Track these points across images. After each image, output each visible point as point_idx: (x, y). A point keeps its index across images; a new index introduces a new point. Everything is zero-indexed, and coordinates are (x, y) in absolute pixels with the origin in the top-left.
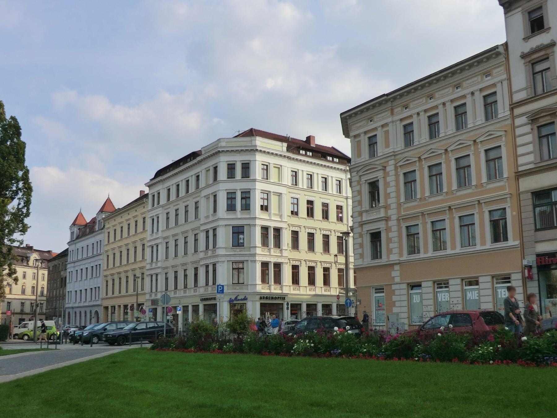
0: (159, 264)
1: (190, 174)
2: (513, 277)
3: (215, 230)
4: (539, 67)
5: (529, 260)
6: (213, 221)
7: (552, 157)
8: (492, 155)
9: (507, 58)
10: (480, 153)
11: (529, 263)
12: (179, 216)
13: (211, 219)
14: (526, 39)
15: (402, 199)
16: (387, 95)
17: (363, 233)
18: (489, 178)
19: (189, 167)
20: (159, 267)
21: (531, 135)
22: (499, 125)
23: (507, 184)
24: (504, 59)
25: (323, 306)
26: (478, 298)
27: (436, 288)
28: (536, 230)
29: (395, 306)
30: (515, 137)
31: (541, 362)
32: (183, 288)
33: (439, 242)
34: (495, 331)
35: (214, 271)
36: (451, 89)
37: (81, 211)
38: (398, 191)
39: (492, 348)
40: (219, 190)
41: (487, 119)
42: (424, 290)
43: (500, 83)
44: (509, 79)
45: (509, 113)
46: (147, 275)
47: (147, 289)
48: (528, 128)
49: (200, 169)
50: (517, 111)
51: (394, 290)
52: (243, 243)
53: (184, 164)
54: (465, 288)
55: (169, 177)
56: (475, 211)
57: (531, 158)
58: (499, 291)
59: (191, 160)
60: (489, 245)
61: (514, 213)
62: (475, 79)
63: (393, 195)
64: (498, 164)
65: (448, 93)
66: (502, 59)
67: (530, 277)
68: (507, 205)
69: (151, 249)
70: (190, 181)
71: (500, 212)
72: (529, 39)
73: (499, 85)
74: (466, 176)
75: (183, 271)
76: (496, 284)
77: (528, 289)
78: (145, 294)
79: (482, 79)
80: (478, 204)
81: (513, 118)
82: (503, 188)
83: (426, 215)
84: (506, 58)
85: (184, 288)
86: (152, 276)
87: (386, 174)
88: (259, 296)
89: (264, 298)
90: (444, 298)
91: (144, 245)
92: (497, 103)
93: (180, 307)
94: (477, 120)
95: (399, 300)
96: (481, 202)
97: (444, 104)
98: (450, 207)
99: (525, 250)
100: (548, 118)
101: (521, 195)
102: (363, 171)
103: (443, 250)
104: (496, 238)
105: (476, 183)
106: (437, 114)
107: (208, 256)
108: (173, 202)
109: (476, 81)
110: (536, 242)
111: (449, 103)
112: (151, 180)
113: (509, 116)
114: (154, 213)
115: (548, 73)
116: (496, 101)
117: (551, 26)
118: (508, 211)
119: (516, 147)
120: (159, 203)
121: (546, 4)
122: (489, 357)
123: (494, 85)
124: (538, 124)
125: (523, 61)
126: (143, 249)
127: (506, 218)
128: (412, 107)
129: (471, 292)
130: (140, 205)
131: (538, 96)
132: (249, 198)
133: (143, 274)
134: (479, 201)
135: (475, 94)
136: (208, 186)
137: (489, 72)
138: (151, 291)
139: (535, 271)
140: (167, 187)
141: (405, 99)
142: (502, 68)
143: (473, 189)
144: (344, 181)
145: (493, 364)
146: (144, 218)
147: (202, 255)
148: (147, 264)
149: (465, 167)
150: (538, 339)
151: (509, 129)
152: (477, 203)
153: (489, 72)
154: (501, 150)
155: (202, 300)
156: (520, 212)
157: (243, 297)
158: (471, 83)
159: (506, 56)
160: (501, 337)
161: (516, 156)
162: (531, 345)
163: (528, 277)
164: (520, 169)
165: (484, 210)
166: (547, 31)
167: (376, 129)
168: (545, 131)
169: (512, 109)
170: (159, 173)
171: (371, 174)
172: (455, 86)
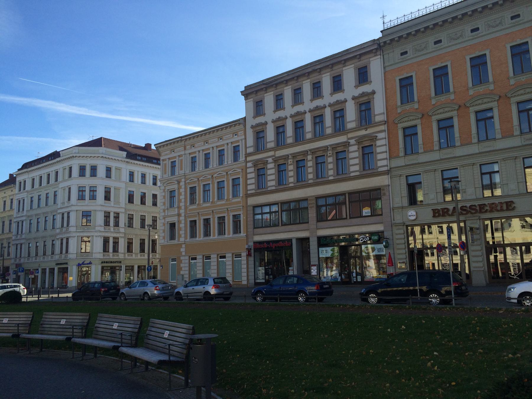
0: (23, 236)
1: (52, 170)
3: (68, 213)
6: (67, 207)
9: (245, 126)
12: (49, 199)
13: (66, 204)
15: (188, 204)
16: (181, 137)
17: (165, 223)
19: (50, 164)
20: (23, 239)
21: (254, 174)
27: (234, 257)
29: (182, 270)
32: (42, 255)
35: (67, 243)
38: (186, 198)
40: (73, 185)
42: (227, 259)
44: (245, 139)
46: (13, 245)
47: (12, 255)
49: (59, 167)
50: (249, 159)
51: (182, 260)
53: (46, 162)
55: (34, 170)
59: (52, 160)
60: (216, 237)
63: (183, 200)
69: (17, 224)
70: (59, 172)
75: (43, 242)
78: (11, 259)
85: (52, 254)
86: (17, 245)
89: (104, 262)
91: (11, 221)
93: (40, 270)
95: (184, 266)
97: (227, 144)
98: (213, 211)
107: (63, 232)
108: (36, 189)
112: (19, 170)
114: (20, 196)
117: (266, 113)
118: (242, 216)
120: (24, 189)
121: (264, 100)
126: (10, 224)
130: (8, 188)
132: (96, 191)
133: (9, 243)
134: (213, 211)
136: (64, 180)
138: (16, 257)
139: (252, 251)
140: (68, 166)
146: (12, 199)
147: (58, 231)
148: (13, 236)
155: (57, 264)
156: (247, 218)
157: (88, 262)
161: (247, 185)
164: (249, 192)
167: (175, 157)
169: (246, 157)
170: (26, 166)
171: (171, 186)
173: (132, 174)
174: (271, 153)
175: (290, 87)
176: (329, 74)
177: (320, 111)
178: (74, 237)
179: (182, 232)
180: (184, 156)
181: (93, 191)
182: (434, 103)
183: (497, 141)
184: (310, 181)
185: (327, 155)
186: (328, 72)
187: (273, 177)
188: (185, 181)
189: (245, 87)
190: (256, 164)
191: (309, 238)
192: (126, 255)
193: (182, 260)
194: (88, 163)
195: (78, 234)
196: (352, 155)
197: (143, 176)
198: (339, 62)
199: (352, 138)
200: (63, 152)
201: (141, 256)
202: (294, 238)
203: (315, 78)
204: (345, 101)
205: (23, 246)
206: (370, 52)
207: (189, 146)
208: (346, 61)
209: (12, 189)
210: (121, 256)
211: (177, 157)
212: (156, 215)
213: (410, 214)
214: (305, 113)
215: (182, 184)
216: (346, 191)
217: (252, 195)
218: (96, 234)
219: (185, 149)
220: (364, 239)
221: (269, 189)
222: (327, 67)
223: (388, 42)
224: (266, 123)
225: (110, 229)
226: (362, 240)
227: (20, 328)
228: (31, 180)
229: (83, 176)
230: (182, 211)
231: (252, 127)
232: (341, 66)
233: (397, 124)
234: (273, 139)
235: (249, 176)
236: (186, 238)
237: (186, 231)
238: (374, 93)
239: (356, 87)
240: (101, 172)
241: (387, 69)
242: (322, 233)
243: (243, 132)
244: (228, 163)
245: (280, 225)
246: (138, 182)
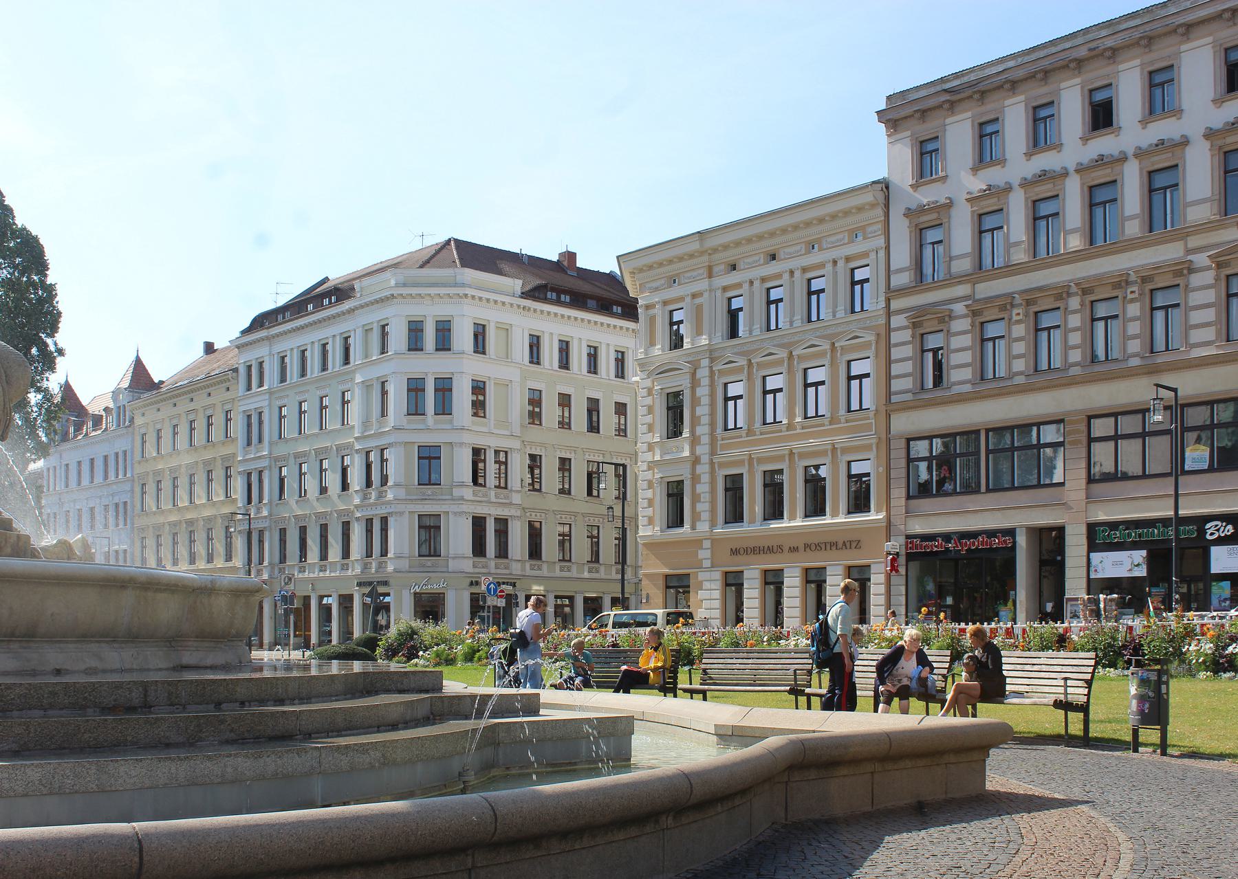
1: (331, 333)
11: (894, 548)
25: (586, 600)
33: (194, 649)
37: (68, 378)
44: (888, 248)
45: (884, 306)
52: (1138, 752)
55: (285, 333)
73: (873, 255)
81: (889, 313)
87: (695, 383)
88: (469, 581)
97: (835, 262)
102: (658, 372)
103: (998, 488)
112: (245, 332)
114: (251, 404)
139: (902, 560)
144: (630, 352)
156: (888, 469)
169: (888, 301)
170: (260, 322)
173: (535, 345)
174: (962, 290)
175: (1022, 98)
176: (1137, 62)
177: (1109, 171)
178: (401, 514)
179: (703, 507)
180: (706, 295)
181: (444, 388)
185: (1125, 298)
188: (711, 367)
190: (917, 319)
192: (527, 566)
193: (701, 582)
194: (430, 313)
195: (411, 507)
196: (1196, 298)
197: (565, 348)
200: (366, 282)
201: (590, 571)
202: (1021, 527)
203: (1097, 74)
204: (1185, 142)
205: (267, 535)
207: (722, 267)
209: (227, 384)
210: (516, 569)
211: (688, 299)
212: (567, 456)
214: (1065, 174)
215: (703, 373)
217: (906, 407)
218: (454, 508)
219: (710, 276)
220: (1218, 530)
221: (956, 389)
222: (1136, 44)
224: (949, 205)
225: (485, 495)
226: (1212, 534)
227: (1070, 690)
228: (276, 361)
229: (416, 350)
230: (703, 450)
231: (909, 213)
232: (1173, 39)
234: (969, 250)
235: (896, 353)
236: (713, 524)
237: (713, 502)
239: (1218, 102)
240: (463, 338)
242: (1102, 515)
243: (880, 226)
244: (834, 316)
245: (983, 489)
246: (551, 364)
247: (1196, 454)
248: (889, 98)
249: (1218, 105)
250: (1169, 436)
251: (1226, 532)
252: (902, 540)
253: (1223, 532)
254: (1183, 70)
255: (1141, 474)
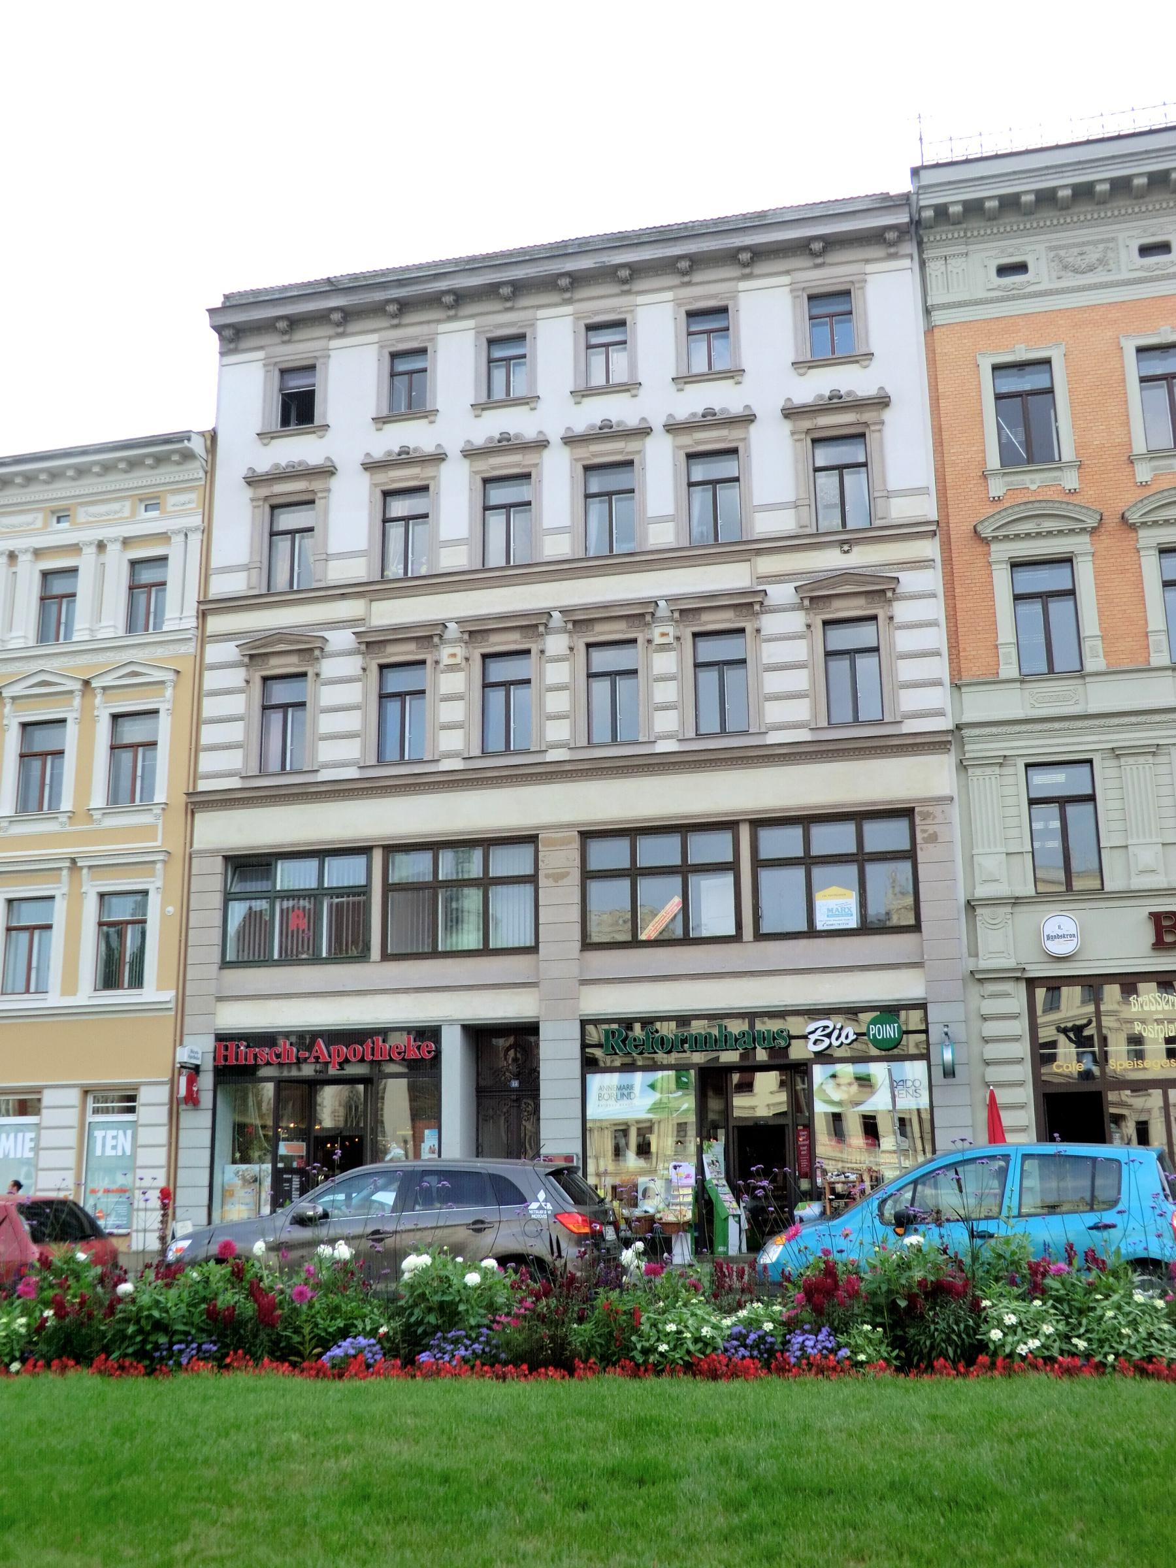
2: (144, 1095)
4: (288, 520)
5: (195, 1049)
7: (288, 768)
8: (133, 732)
9: (210, 472)
10: (95, 722)
14: (265, 436)
18: (114, 797)
21: (242, 697)
22: (160, 651)
23: (160, 822)
24: (201, 474)
26: (31, 1155)
28: (225, 964)
30: (199, 695)
31: (162, 1358)
34: (45, 1263)
36: (40, 516)
39: (23, 1320)
41: (131, 627)
43: (181, 537)
44: (207, 531)
48: (237, 677)
50: (216, 624)
54: (91, 1118)
56: (58, 888)
57: (800, 710)
58: (99, 1134)
60: (86, 993)
61: (170, 909)
62: (115, 506)
64: (144, 761)
65: (120, 515)
66: (195, 470)
67: (192, 1099)
68: (153, 884)
71: (130, 901)
72: (272, 438)
73: (178, 540)
74: (48, 781)
76: (94, 1113)
77: (182, 1133)
79: (134, 513)
80: (69, 868)
82: (146, 832)
83: (85, 871)
84: (206, 473)
90: (114, 1147)
92: (165, 590)
94: (103, 624)
96: (79, 864)
97: (101, 546)
99: (187, 1018)
100: (294, 659)
101: (195, 861)
104: (110, 978)
105: (74, 806)
106: (164, 559)
109: (116, 512)
110: (220, 999)
111: (117, 546)
113: (193, 632)
115: (307, 542)
116: (164, 584)
119: (198, 722)
121: (326, 364)
122: (12, 1350)
123: (164, 537)
124: (829, 613)
125: (248, 493)
127: (144, 922)
128: (83, 520)
129: (12, 1136)
131: (298, 591)
135: (84, 552)
137: (158, 498)
139: (206, 1081)
141: (62, 490)
142: (193, 496)
143: (61, 823)
145: (18, 1372)
149: (47, 754)
150: (164, 1290)
151: (187, 668)
152: (68, 864)
153: (158, 498)
154: (158, 723)
156: (186, 910)
158: (102, 515)
159: (209, 469)
160: (61, 1286)
161: (196, 749)
162: (140, 1309)
163: (185, 1098)
164: (203, 786)
165: (83, 890)
166: (320, 433)
168: (501, 671)
169: (203, 615)
172: (53, 512)
182: (1148, 478)
183: (1088, 679)
184: (663, 747)
186: (670, 288)
187: (351, 721)
189: (226, 297)
191: (538, 1023)
196: (772, 653)
198: (731, 257)
199: (779, 578)
202: (451, 1022)
204: (327, 471)
206: (875, 237)
208: (759, 254)
213: (1051, 928)
216: (375, 840)
220: (829, 1036)
222: (378, 310)
223: (955, 209)
233: (986, 542)
234: (566, 521)
238: (882, 402)
239: (265, 436)
241: (938, 317)
247: (833, 903)
248: (226, 297)
249: (266, 441)
250: (729, 878)
251: (842, 1039)
252: (209, 1044)
253: (837, 1039)
254: (540, 343)
255: (855, 926)
